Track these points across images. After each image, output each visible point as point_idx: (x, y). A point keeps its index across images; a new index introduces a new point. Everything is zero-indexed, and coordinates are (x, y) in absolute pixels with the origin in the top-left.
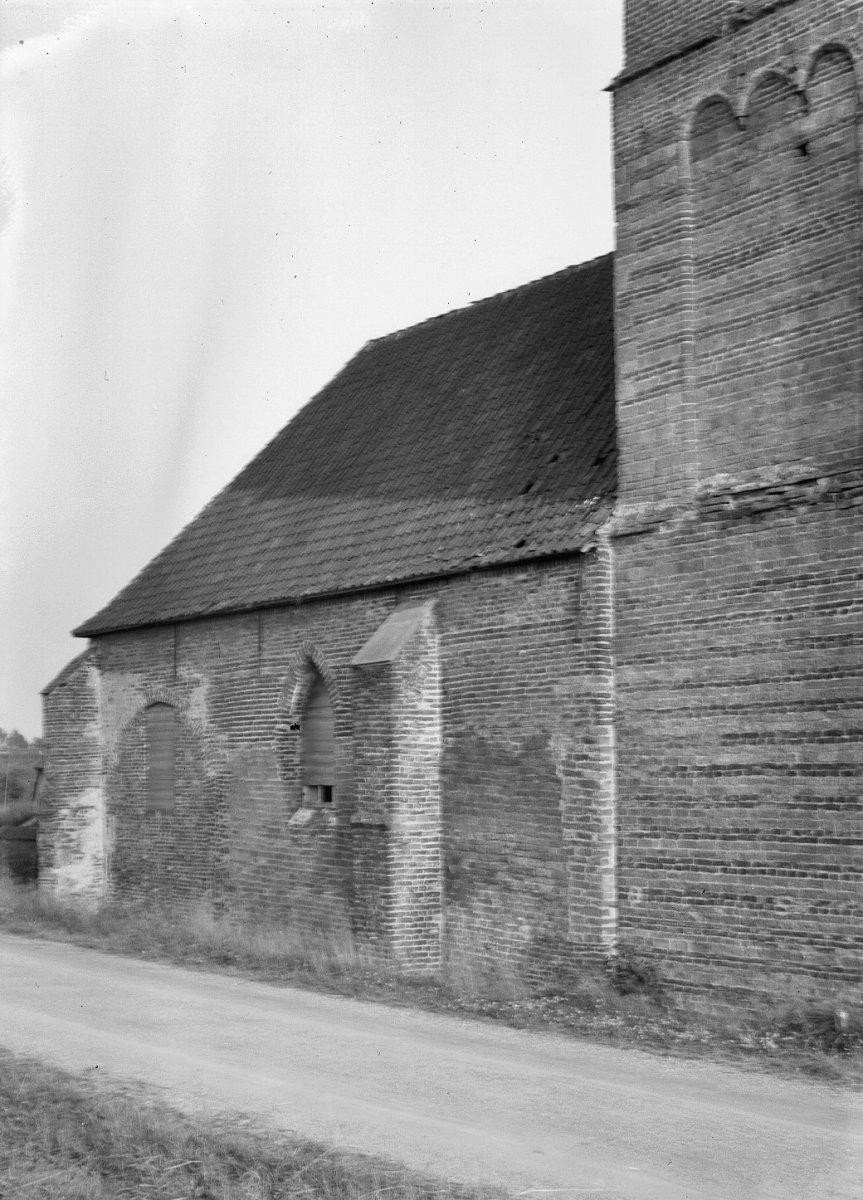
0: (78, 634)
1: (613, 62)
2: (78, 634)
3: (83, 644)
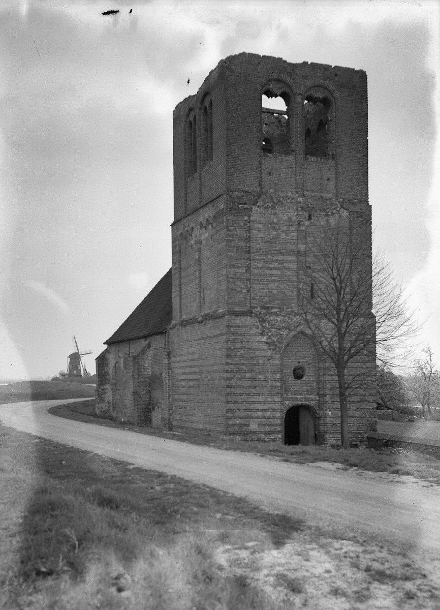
0: (104, 343)
1: (172, 220)
2: (104, 343)
3: (106, 346)
